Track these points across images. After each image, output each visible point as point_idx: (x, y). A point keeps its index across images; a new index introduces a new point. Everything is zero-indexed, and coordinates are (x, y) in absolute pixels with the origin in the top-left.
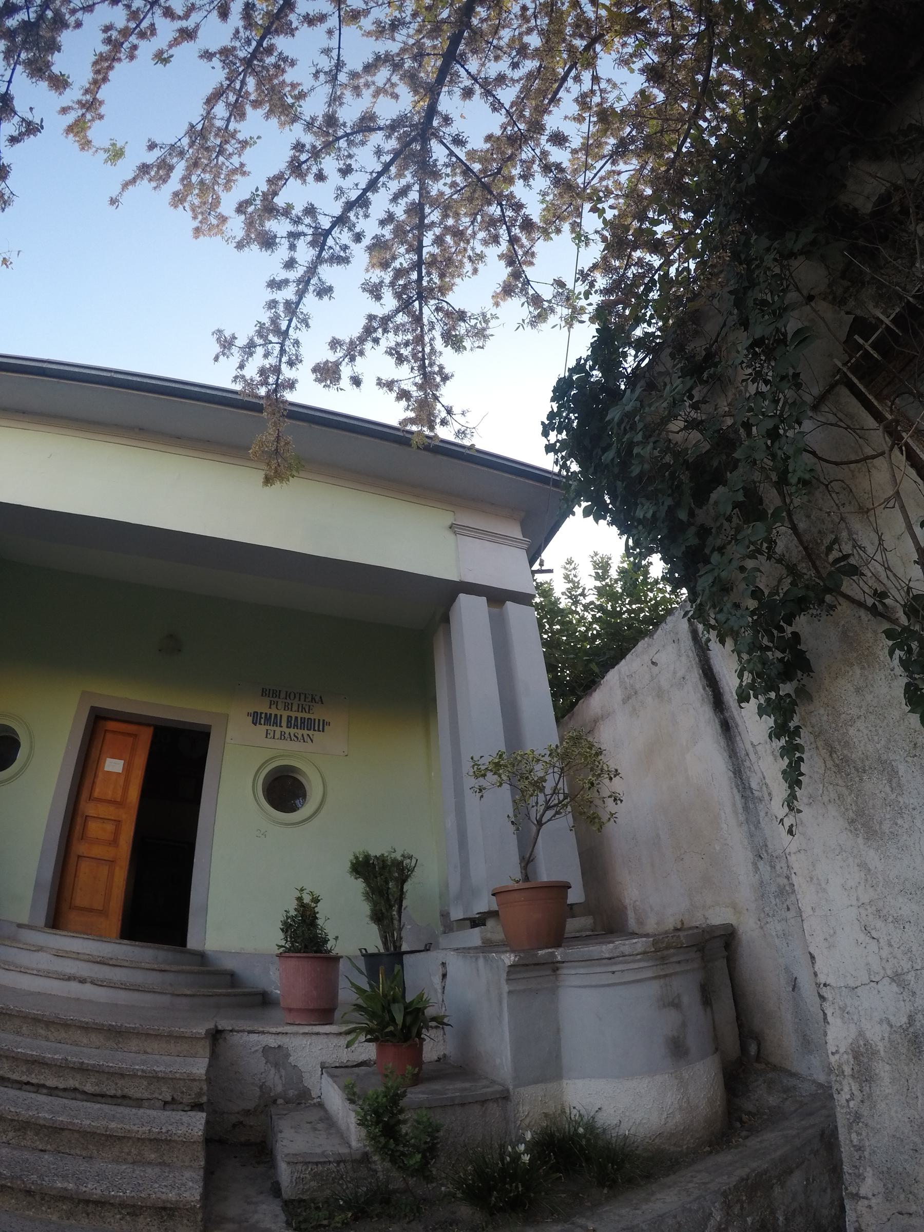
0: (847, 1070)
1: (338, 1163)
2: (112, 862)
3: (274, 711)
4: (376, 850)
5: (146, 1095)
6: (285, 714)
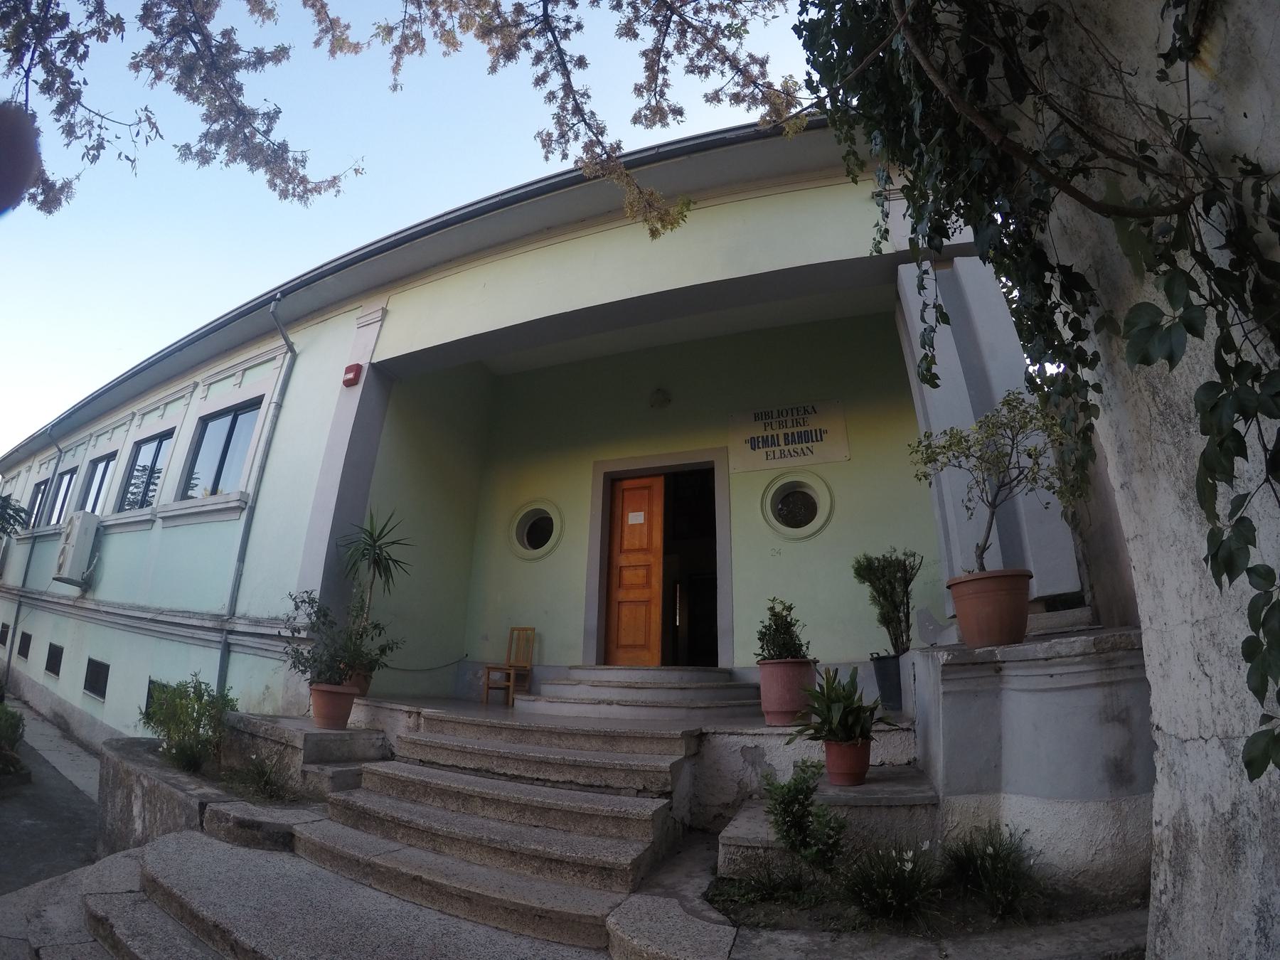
0: (1166, 855)
1: (766, 849)
2: (648, 602)
3: (769, 432)
4: (877, 552)
5: (624, 785)
6: (781, 433)
